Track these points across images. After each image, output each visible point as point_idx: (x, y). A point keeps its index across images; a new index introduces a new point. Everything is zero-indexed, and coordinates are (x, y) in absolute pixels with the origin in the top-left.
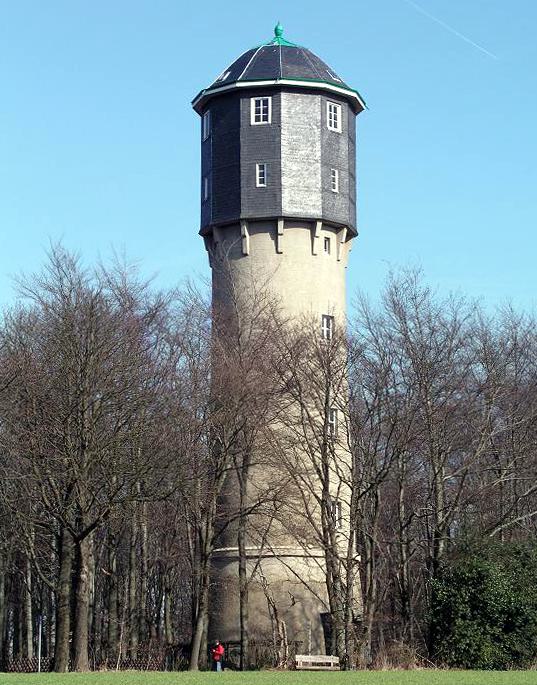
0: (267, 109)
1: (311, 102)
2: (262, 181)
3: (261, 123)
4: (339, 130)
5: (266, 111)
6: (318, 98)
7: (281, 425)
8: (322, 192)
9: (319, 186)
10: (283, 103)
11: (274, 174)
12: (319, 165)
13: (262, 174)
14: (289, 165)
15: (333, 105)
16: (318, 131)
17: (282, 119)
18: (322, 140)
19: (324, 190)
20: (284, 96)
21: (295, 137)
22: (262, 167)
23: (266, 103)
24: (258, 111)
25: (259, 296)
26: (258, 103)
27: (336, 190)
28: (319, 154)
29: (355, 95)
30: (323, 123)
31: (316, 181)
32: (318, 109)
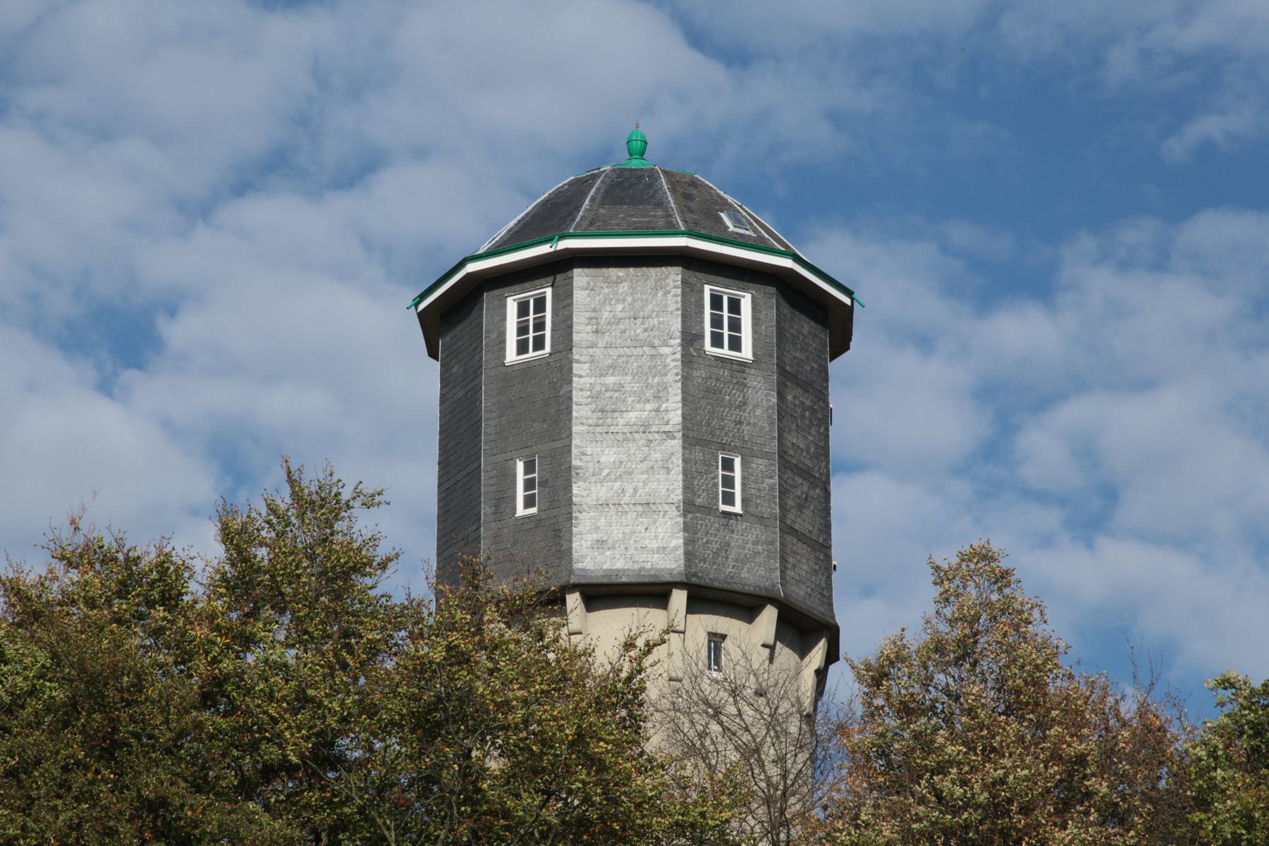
0: (543, 337)
1: (655, 289)
2: (529, 502)
3: (531, 354)
4: (747, 353)
5: (735, 325)
6: (674, 275)
7: (259, 808)
8: (686, 512)
9: (678, 496)
10: (579, 296)
11: (555, 484)
12: (676, 444)
13: (529, 485)
14: (590, 449)
15: (727, 293)
16: (672, 353)
17: (576, 337)
18: (686, 380)
19: (689, 507)
20: (580, 277)
21: (610, 380)
22: (529, 468)
23: (735, 306)
24: (522, 330)
25: (600, 573)
26: (523, 309)
27: (737, 508)
28: (676, 417)
29: (787, 263)
30: (691, 338)
31: (671, 485)
32: (674, 301)
